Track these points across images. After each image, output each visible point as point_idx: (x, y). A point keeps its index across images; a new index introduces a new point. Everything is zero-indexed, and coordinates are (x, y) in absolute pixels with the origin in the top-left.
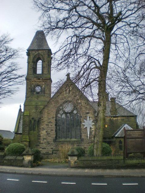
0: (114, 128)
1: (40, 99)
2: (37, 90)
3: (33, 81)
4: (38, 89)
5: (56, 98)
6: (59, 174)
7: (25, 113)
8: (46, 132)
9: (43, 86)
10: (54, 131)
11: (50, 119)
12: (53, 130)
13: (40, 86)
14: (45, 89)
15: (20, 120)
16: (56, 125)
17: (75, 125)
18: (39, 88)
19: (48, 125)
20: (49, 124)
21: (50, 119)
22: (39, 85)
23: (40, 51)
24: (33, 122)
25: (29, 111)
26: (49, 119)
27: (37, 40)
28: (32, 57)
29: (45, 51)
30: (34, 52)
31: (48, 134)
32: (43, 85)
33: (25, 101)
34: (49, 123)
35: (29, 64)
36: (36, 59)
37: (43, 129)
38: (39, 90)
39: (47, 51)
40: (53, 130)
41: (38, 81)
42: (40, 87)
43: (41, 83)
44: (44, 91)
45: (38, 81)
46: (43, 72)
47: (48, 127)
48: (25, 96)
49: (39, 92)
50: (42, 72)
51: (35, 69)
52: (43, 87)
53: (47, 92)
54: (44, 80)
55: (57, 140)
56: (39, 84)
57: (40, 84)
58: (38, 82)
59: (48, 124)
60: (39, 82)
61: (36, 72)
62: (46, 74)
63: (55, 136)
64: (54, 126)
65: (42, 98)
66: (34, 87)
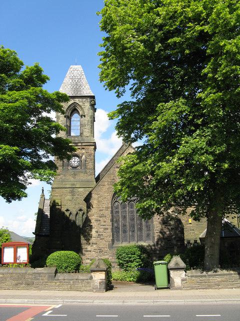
0: (202, 224)
1: (77, 178)
2: (73, 163)
4: (75, 161)
6: (206, 259)
10: (110, 230)
12: (107, 229)
16: (112, 220)
17: (136, 228)
18: (76, 160)
20: (101, 219)
23: (77, 100)
26: (100, 210)
27: (71, 81)
38: (76, 163)
40: (107, 229)
42: (77, 158)
44: (85, 165)
50: (11, 247)
53: (90, 165)
55: (114, 246)
59: (99, 218)
61: (70, 133)
62: (88, 137)
64: (109, 222)
65: (82, 177)
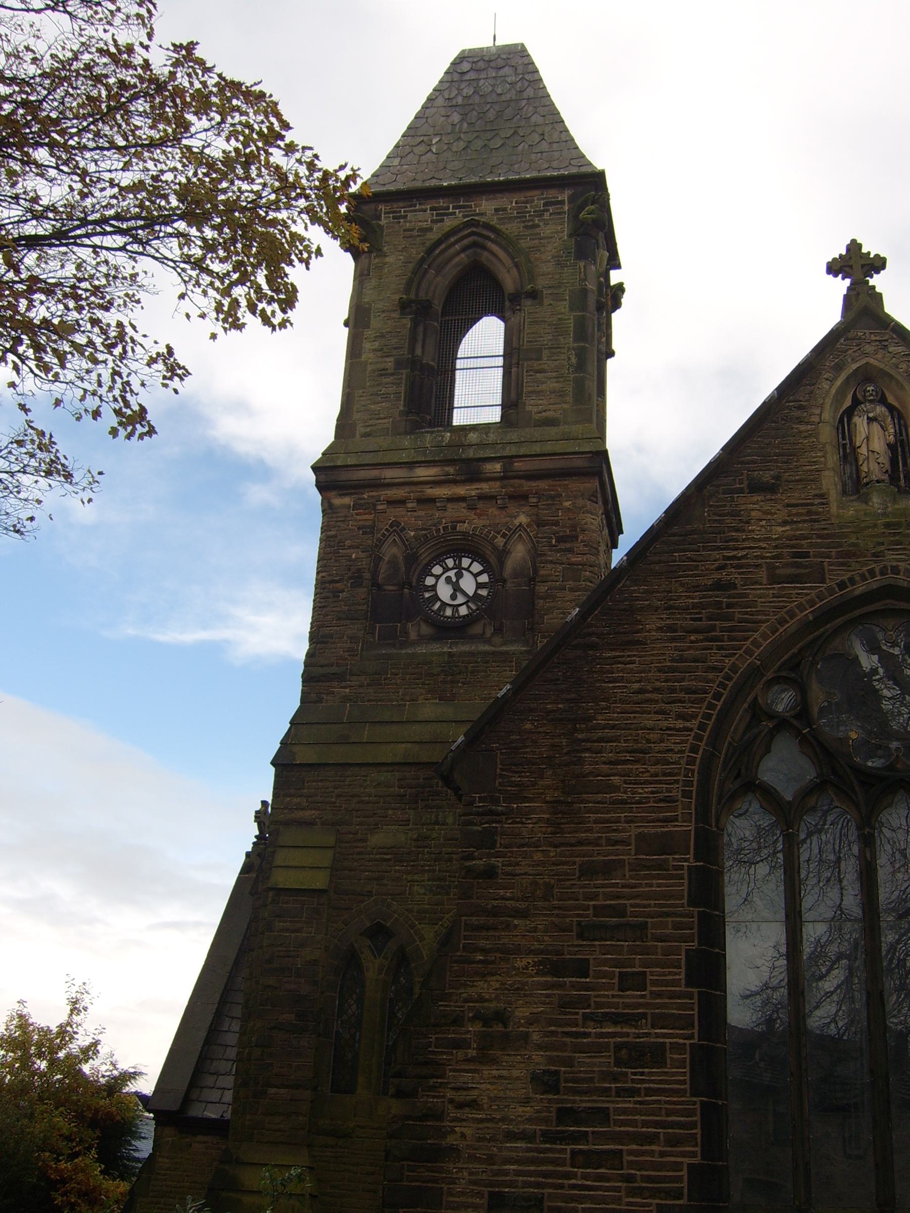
3: (402, 502)
5: (556, 966)
7: (282, 857)
8: (547, 1082)
9: (519, 552)
10: (677, 1073)
11: (608, 869)
12: (655, 1055)
13: (476, 556)
14: (532, 580)
15: (219, 1015)
19: (582, 969)
21: (608, 869)
22: (461, 546)
23: (486, 207)
24: (373, 968)
25: (331, 840)
26: (588, 871)
27: (456, 118)
28: (395, 261)
29: (538, 199)
30: (421, 216)
31: (566, 1114)
32: (511, 533)
33: (324, 529)
34: (584, 932)
35: (368, 333)
36: (437, 285)
37: (498, 1035)
39: (565, 196)
40: (655, 1055)
41: (461, 491)
42: (477, 567)
43: (493, 511)
45: (461, 491)
46: (511, 402)
47: (584, 1002)
48: (308, 628)
49: (469, 620)
51: (429, 386)
52: (510, 564)
54: (527, 485)
56: (472, 523)
57: (479, 522)
58: (455, 511)
60: (471, 503)
63: (690, 1155)
66: (411, 559)
